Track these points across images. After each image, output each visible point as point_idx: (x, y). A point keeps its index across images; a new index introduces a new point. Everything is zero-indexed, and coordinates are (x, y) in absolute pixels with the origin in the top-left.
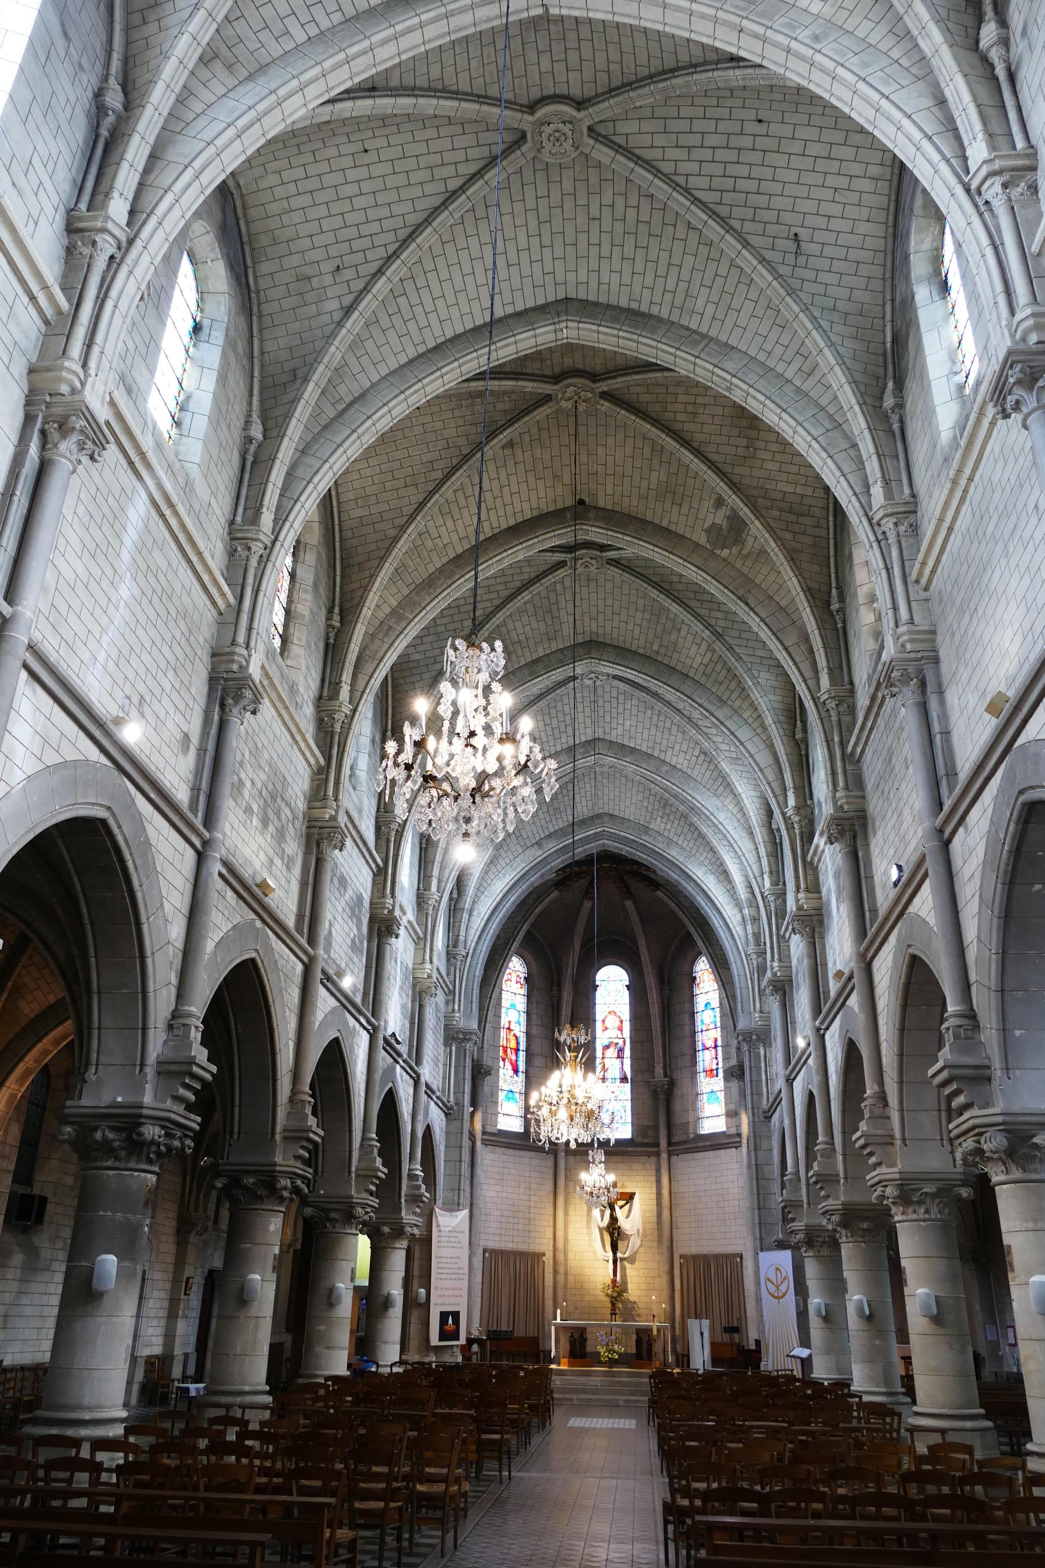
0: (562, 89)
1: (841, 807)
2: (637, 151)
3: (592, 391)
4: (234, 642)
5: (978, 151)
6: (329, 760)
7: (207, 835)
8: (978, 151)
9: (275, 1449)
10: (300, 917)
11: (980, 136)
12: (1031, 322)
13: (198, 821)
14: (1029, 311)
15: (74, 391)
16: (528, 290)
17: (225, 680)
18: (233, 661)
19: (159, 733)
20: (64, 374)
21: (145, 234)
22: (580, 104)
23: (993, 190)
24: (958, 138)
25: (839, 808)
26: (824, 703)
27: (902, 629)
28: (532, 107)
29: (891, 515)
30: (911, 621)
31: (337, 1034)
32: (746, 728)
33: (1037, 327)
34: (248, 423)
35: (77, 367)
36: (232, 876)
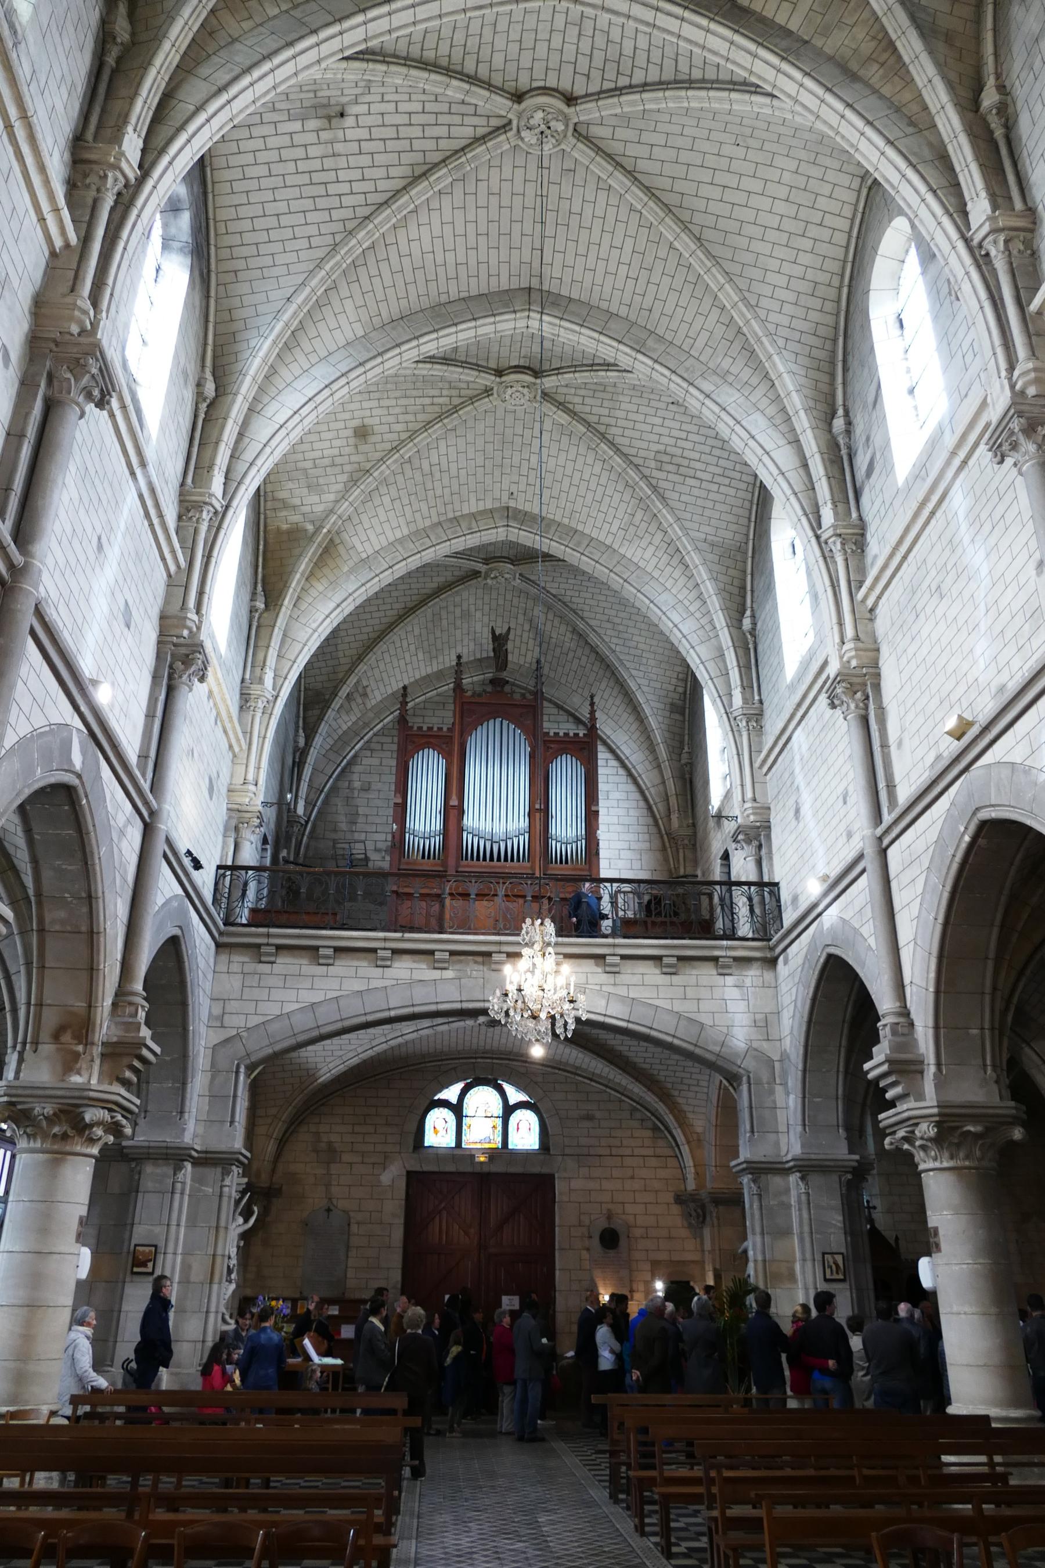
0: (552, 82)
1: (1023, 393)
2: (617, 158)
3: (566, 120)
4: (184, 606)
5: (980, 209)
6: (86, 240)
7: (18, 559)
8: (980, 209)
9: (348, 1320)
10: (143, 757)
11: (983, 194)
12: (853, 653)
13: (146, 786)
14: (1030, 365)
15: (83, 332)
16: (473, 501)
17: (175, 645)
18: (71, 318)
19: (123, 696)
20: (77, 313)
21: (156, 173)
22: (570, 100)
23: (836, 546)
24: (960, 195)
25: (1018, 396)
26: (980, 246)
27: (748, 805)
28: (518, 97)
29: (1002, 230)
30: (755, 800)
31: (177, 931)
32: (757, 416)
33: (1037, 381)
34: (296, 735)
35: (87, 305)
36: (172, 856)
